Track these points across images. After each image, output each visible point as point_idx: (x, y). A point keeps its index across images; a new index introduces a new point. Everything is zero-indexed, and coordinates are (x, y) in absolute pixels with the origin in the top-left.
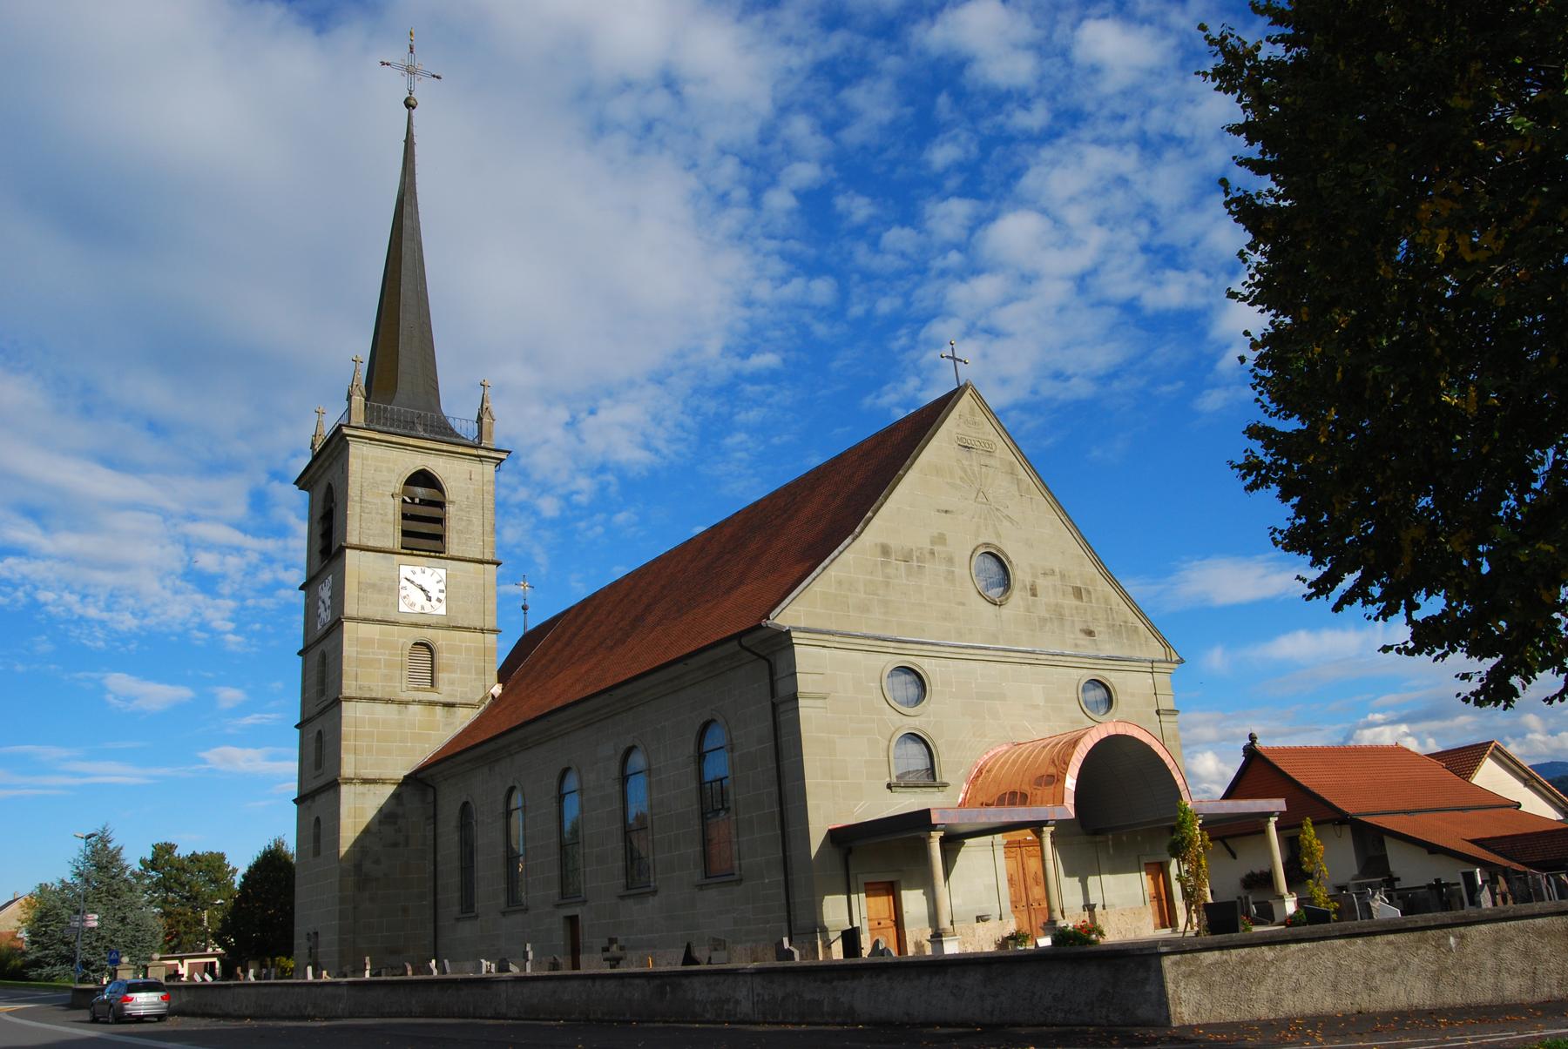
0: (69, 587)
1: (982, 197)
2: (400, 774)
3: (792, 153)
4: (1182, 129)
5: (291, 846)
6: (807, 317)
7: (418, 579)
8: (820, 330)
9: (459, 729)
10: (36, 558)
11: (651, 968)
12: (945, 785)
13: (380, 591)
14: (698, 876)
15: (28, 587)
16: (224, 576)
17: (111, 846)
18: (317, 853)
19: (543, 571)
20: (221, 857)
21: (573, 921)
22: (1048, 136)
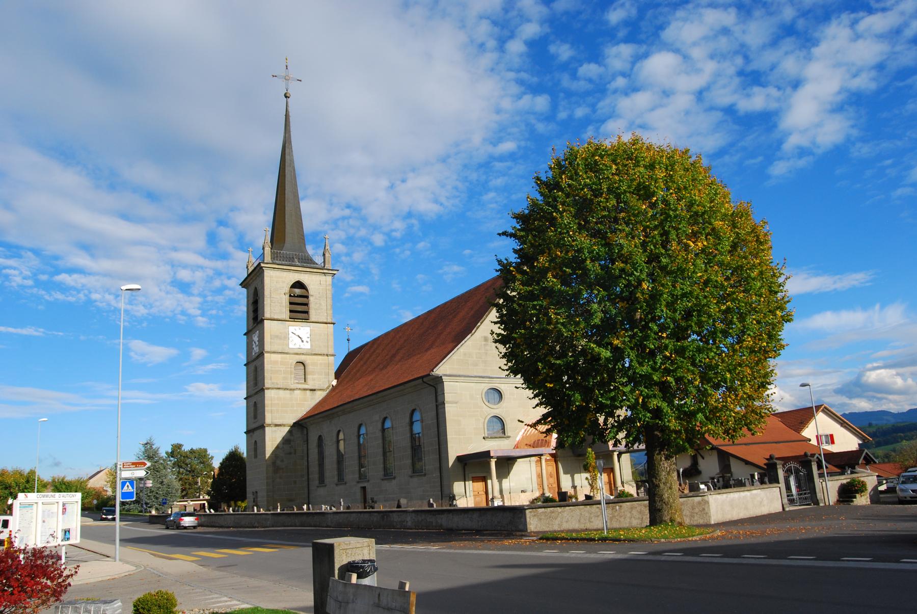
0: (108, 291)
1: (639, 42)
2: (292, 422)
3: (524, 19)
5: (243, 450)
6: (532, 120)
8: (541, 127)
9: (318, 401)
10: (90, 274)
11: (382, 509)
12: (509, 437)
14: (410, 472)
15: (86, 292)
16: (194, 283)
17: (154, 447)
18: (256, 456)
20: (206, 450)
21: (364, 488)
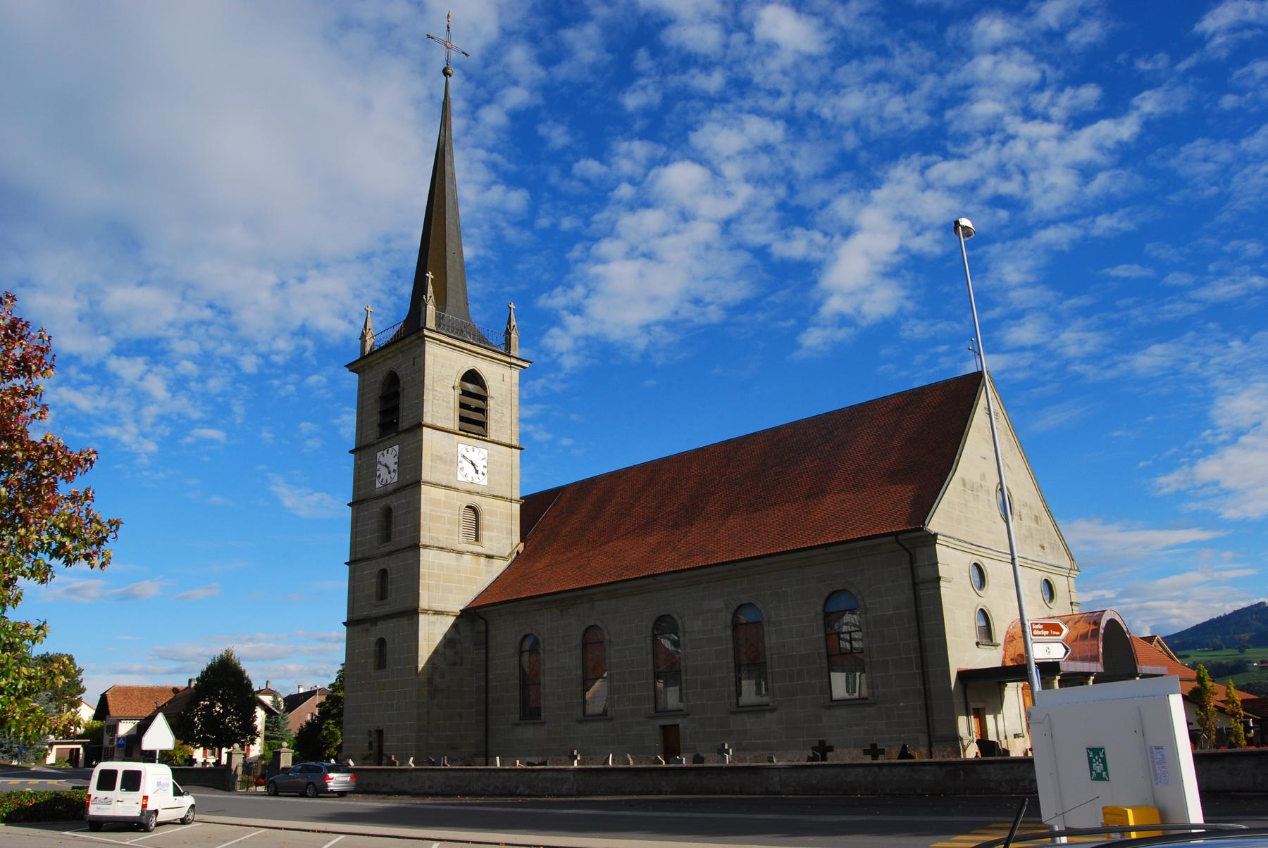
2: (457, 607)
4: (826, 112)
7: (470, 456)
8: (511, 234)
13: (445, 463)
19: (239, 420)
22: (720, 99)
